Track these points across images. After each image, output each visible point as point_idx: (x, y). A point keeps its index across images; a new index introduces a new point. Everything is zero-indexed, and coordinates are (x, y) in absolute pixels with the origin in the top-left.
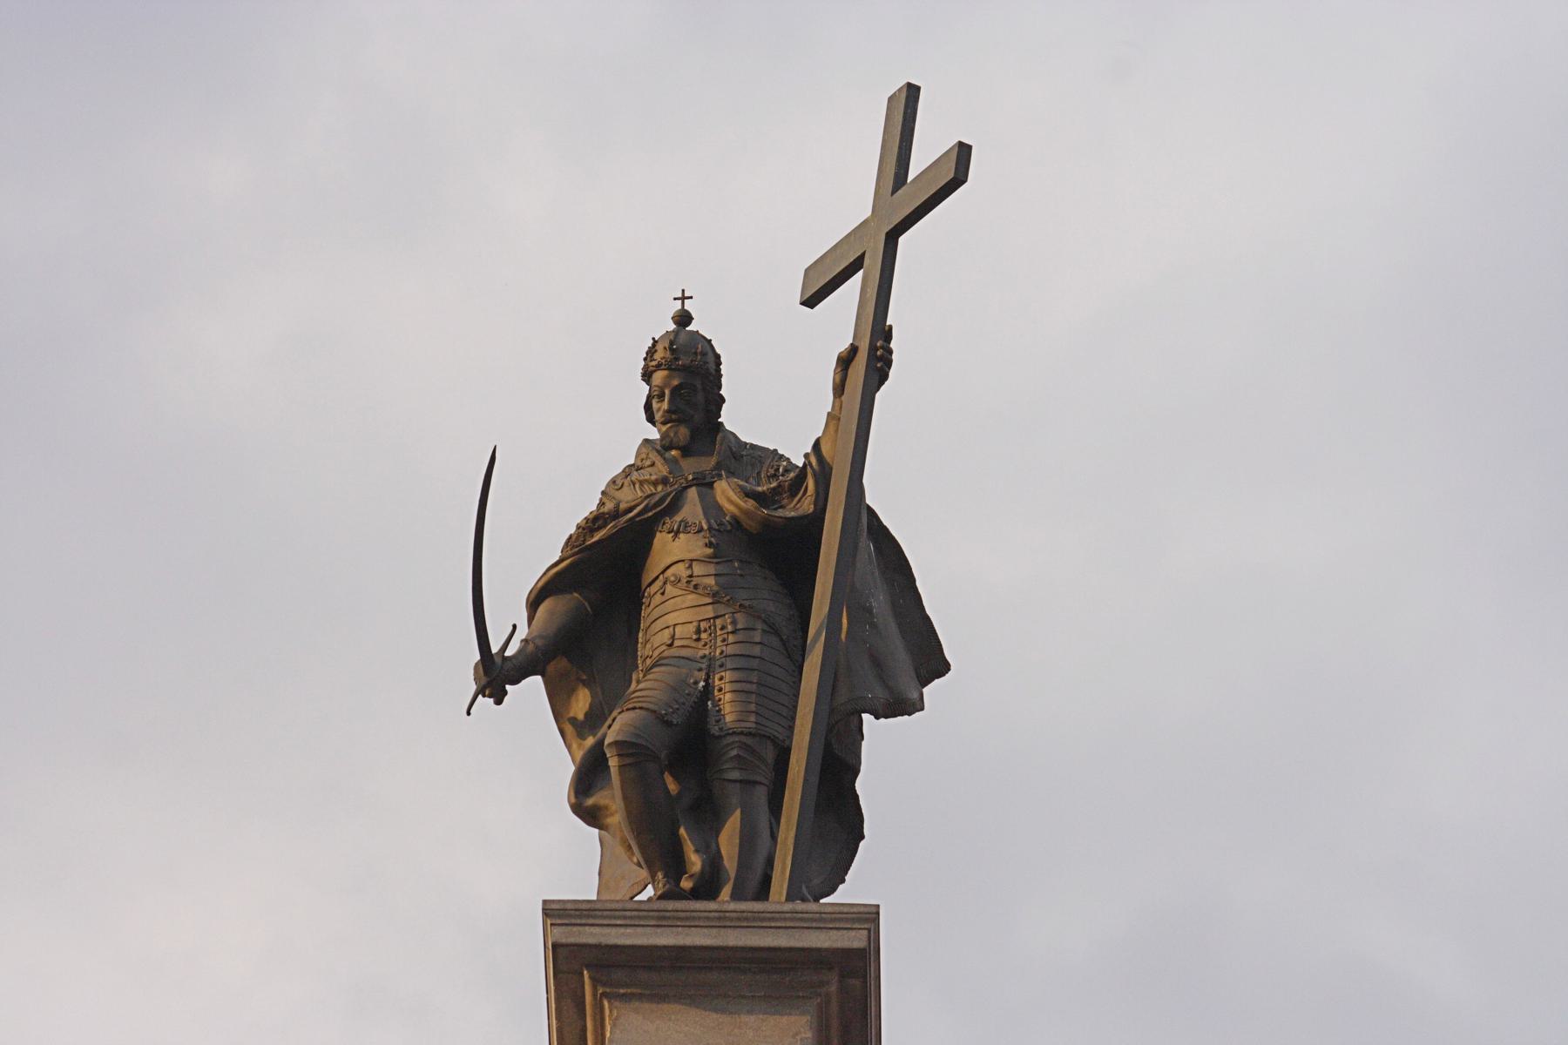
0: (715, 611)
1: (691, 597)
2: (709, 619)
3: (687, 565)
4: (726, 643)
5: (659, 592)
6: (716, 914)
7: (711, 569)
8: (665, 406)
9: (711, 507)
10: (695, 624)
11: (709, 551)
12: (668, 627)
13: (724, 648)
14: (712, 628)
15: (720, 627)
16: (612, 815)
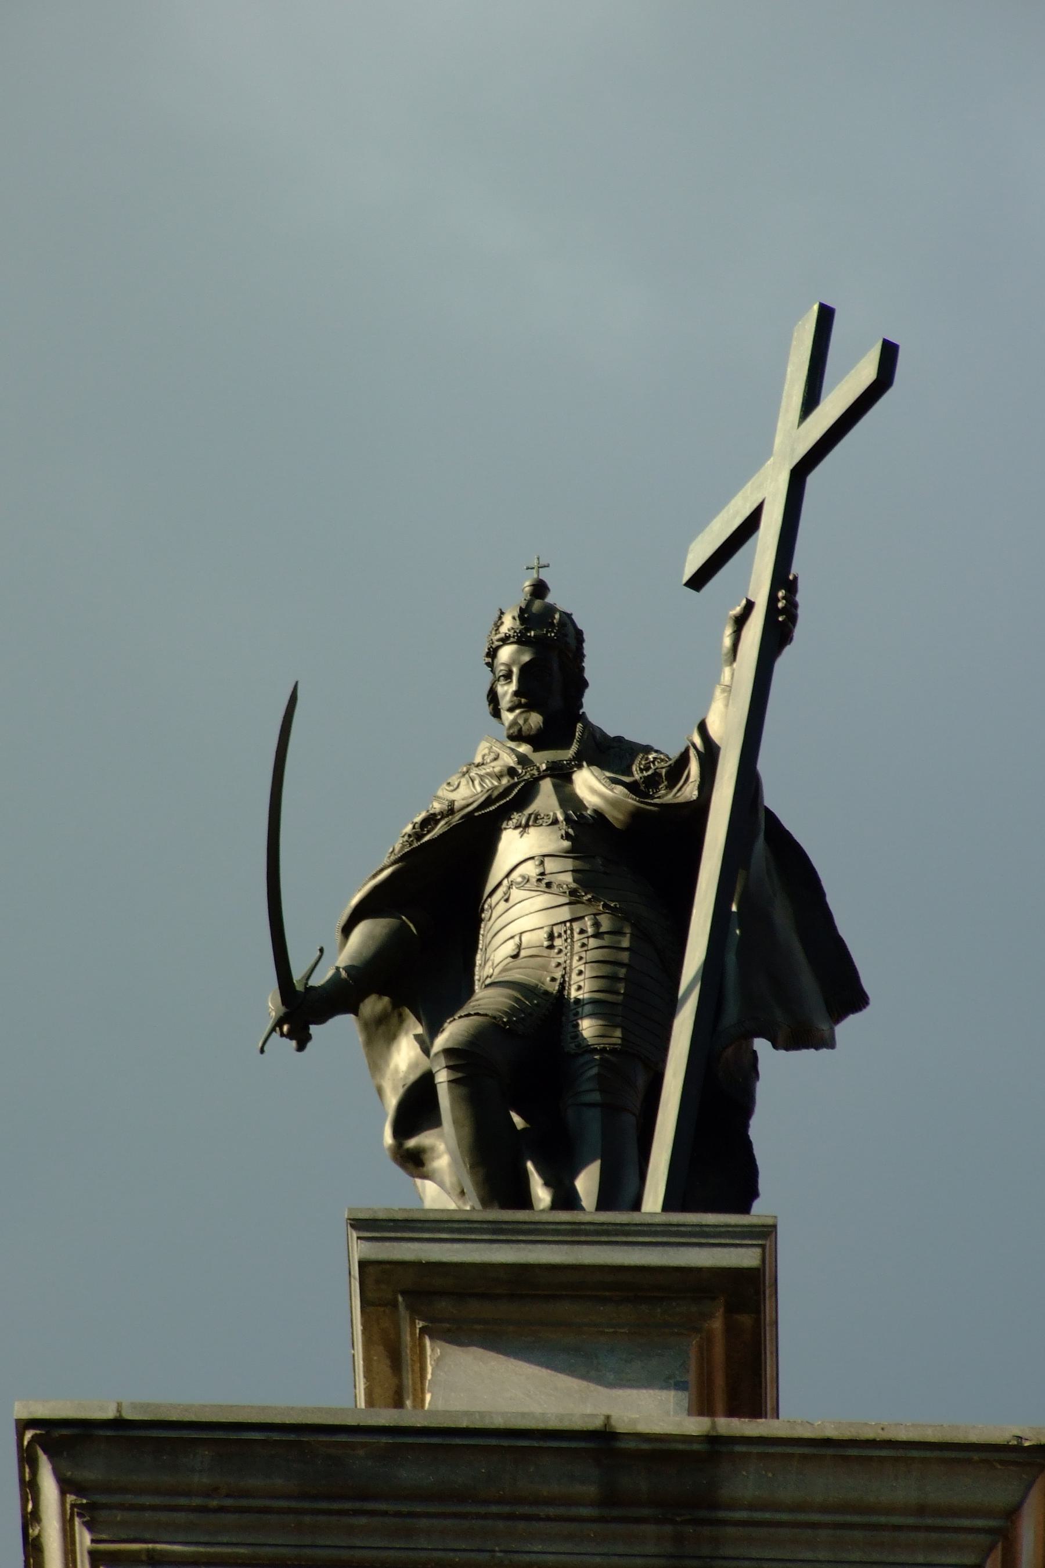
0: (572, 912)
1: (546, 897)
2: (564, 922)
3: (537, 863)
4: (586, 948)
5: (503, 899)
6: (569, 1227)
7: (569, 864)
8: (513, 687)
9: (569, 800)
10: (546, 929)
11: (566, 844)
12: (512, 937)
13: (583, 955)
14: (569, 932)
15: (578, 930)
16: (439, 1157)
